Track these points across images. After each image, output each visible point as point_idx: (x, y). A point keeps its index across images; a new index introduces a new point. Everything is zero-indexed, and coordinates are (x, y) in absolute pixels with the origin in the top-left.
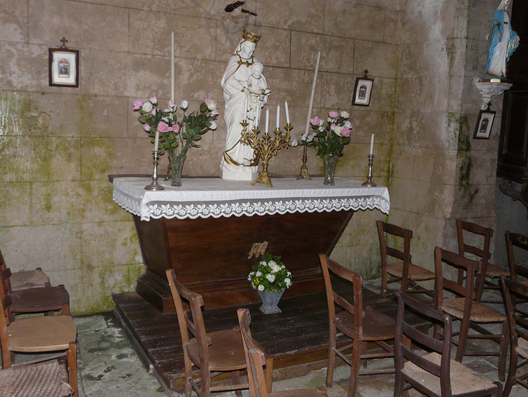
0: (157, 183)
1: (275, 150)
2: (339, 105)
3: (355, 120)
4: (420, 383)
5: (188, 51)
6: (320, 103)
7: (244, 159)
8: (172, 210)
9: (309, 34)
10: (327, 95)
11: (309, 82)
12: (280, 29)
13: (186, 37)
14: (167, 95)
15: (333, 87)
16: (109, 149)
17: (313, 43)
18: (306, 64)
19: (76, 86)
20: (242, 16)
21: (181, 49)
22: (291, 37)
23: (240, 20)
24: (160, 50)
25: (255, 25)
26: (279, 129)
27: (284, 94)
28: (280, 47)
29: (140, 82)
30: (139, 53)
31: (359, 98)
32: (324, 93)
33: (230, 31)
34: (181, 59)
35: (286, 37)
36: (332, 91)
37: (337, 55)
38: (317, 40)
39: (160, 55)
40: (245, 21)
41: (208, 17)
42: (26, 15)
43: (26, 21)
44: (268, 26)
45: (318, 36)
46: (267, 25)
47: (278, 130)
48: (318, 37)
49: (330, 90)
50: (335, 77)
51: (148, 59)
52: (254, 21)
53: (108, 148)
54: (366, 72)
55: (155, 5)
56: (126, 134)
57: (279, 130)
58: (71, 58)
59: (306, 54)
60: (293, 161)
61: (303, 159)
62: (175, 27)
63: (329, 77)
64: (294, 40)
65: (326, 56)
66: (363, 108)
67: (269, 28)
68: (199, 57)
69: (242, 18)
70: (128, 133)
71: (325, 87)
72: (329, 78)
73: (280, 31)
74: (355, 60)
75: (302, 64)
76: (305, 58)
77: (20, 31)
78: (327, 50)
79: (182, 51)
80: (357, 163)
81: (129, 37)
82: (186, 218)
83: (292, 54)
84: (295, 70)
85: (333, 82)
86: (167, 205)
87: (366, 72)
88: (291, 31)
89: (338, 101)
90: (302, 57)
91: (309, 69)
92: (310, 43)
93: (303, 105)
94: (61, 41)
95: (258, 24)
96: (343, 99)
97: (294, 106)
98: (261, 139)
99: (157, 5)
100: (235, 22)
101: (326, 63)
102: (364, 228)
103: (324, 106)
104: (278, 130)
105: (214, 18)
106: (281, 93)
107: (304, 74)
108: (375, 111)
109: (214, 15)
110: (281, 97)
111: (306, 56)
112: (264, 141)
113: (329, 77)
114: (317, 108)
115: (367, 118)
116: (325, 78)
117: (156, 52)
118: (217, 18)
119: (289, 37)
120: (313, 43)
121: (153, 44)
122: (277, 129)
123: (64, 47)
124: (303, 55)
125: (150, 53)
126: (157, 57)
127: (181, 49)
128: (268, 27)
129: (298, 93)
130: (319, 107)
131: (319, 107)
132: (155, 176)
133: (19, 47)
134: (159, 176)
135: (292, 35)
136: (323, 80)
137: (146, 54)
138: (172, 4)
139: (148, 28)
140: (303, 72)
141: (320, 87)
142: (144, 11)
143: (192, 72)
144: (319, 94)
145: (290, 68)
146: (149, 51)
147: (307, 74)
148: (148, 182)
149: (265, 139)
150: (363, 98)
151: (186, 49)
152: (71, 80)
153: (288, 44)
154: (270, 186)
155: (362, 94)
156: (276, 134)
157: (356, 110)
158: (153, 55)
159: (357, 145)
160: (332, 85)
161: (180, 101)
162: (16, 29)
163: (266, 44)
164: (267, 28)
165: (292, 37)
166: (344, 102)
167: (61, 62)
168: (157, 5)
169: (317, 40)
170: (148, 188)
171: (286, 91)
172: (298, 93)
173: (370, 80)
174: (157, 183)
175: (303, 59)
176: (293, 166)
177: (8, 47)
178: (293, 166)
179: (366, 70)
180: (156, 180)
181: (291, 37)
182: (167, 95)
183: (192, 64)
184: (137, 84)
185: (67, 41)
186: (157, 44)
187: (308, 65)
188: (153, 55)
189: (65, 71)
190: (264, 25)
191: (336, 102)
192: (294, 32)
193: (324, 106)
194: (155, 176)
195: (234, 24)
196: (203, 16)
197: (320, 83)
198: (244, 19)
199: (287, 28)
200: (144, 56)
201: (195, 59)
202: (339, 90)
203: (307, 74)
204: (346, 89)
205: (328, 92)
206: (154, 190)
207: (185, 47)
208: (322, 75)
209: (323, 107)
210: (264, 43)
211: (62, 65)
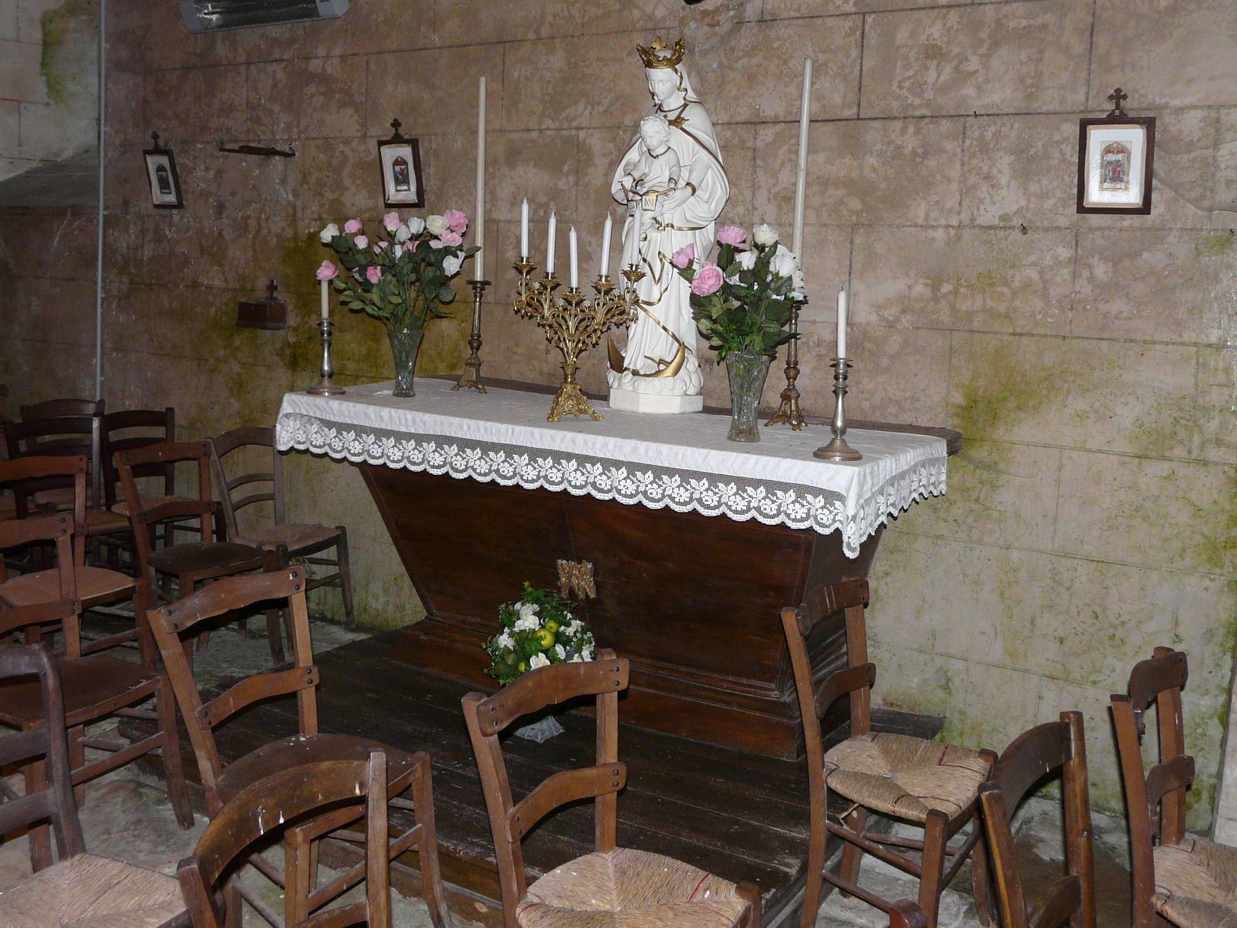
0: (843, 441)
1: (595, 331)
2: (1029, 216)
3: (1095, 261)
4: (272, 827)
5: (605, 112)
6: (959, 213)
7: (645, 357)
8: (687, 490)
9: (923, 12)
10: (984, 187)
11: (920, 151)
12: (831, 16)
13: (603, 80)
14: (564, 213)
15: (1004, 163)
16: (463, 325)
17: (937, 35)
18: (909, 101)
19: (1082, 209)
20: (728, 6)
21: (593, 108)
22: (863, 33)
23: (722, 18)
24: (552, 119)
25: (761, 21)
26: (606, 277)
27: (839, 193)
28: (830, 65)
29: (518, 189)
30: (518, 131)
31: (1102, 189)
32: (972, 180)
33: (697, 49)
34: (592, 131)
35: (847, 35)
36: (1000, 171)
37: (1023, 57)
38: (949, 25)
39: (554, 129)
40: (733, 17)
41: (650, 25)
42: (363, 90)
43: (363, 100)
44: (797, 15)
45: (953, 12)
46: (793, 14)
47: (603, 279)
48: (953, 17)
49: (994, 171)
50: (1012, 128)
51: (534, 141)
52: (758, 12)
53: (462, 322)
54: (1118, 96)
55: (547, 25)
56: (493, 296)
57: (606, 281)
58: (1134, 137)
59: (911, 73)
60: (866, 380)
61: (786, 371)
62: (582, 64)
63: (992, 129)
64: (872, 39)
65: (979, 67)
66: (1129, 220)
67: (800, 21)
68: (626, 123)
69: (729, 10)
70: (495, 293)
71: (974, 161)
72: (989, 135)
73: (830, 22)
74: (1094, 67)
75: (895, 104)
76: (907, 84)
77: (356, 118)
78: (984, 49)
79: (595, 113)
80: (1097, 405)
81: (502, 100)
82: (807, 529)
83: (865, 80)
84: (874, 124)
85: (1004, 144)
86: (647, 471)
87: (1118, 96)
88: (864, 14)
89: (1023, 203)
90: (895, 84)
91: (917, 113)
92: (924, 37)
93: (898, 221)
94: (1111, 97)
95: (767, 17)
96: (1043, 196)
97: (870, 226)
98: (561, 302)
99: (550, 23)
100: (710, 25)
101: (979, 89)
102: (1120, 633)
103: (973, 220)
104: (603, 279)
105: (661, 25)
106: (831, 191)
107: (903, 131)
108: (1182, 229)
109: (663, 18)
110: (831, 200)
111: (909, 77)
112: (569, 307)
113: (992, 129)
114: (947, 227)
115: (1145, 255)
116: (977, 134)
117: (549, 123)
118: (668, 24)
119: (858, 33)
120: (937, 35)
121: (541, 107)
122: (601, 277)
123: (1117, 113)
124: (900, 78)
125: (537, 127)
126: (548, 133)
127: (593, 108)
128: (797, 18)
129: (883, 186)
130: (955, 223)
131: (955, 223)
132: (839, 423)
133: (354, 144)
134: (848, 423)
135: (867, 27)
136: (968, 142)
137: (529, 130)
138: (577, 15)
139: (534, 76)
140: (898, 124)
141: (958, 165)
142: (529, 42)
143: (613, 157)
144: (954, 186)
145: (858, 119)
146: (533, 123)
147: (911, 129)
148: (822, 437)
149: (570, 304)
150: (1123, 185)
151: (602, 109)
152: (1131, 195)
153: (855, 53)
154: (743, 436)
155: (1115, 174)
156: (599, 292)
157: (1099, 229)
158: (541, 131)
159: (1104, 346)
160: (1001, 153)
161: (363, 225)
162: (352, 116)
163: (791, 64)
164: (794, 22)
165: (866, 32)
166: (1049, 203)
167: (1108, 150)
168: (550, 23)
169: (949, 25)
170: (821, 453)
171: (848, 184)
172: (883, 186)
173: (408, 142)
174: (843, 441)
175: (901, 87)
176: (866, 395)
177: (341, 148)
178: (866, 395)
179: (1118, 91)
180: (843, 432)
181: (863, 33)
182: (564, 213)
183: (614, 140)
184: (513, 192)
185: (1125, 97)
186: (548, 105)
187: (917, 102)
188: (541, 131)
189: (1115, 174)
190: (785, 15)
191: (1015, 207)
192: (873, 16)
193: (973, 220)
194: (839, 423)
195: (706, 29)
196: (639, 25)
197: (959, 150)
198: (732, 13)
199: (853, 10)
200: (525, 135)
201: (619, 127)
202: (1027, 166)
203: (911, 129)
204: (1054, 162)
205: (988, 177)
206: (838, 459)
207: (599, 103)
208: (965, 127)
209: (967, 222)
210: (785, 62)
211: (1111, 157)
